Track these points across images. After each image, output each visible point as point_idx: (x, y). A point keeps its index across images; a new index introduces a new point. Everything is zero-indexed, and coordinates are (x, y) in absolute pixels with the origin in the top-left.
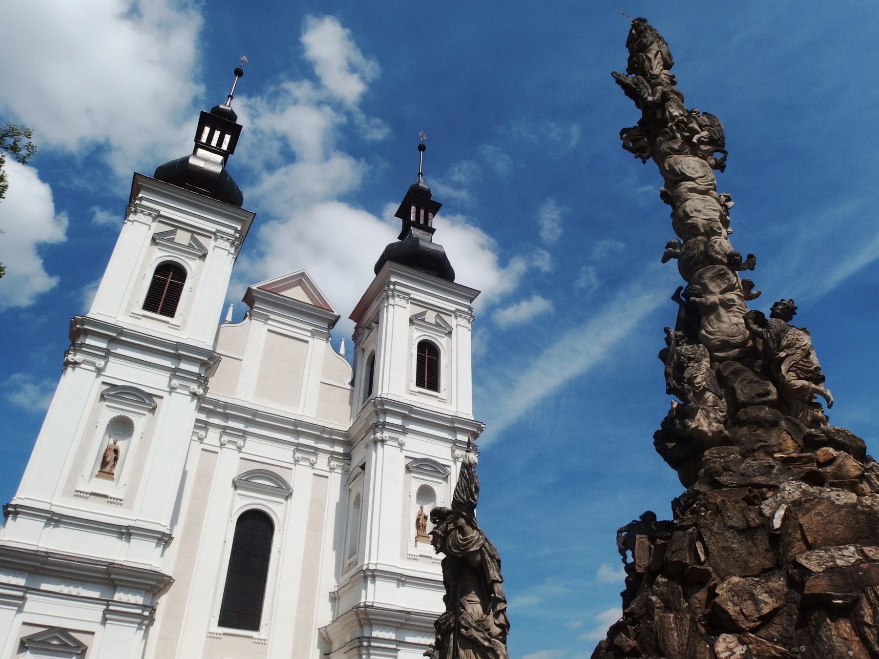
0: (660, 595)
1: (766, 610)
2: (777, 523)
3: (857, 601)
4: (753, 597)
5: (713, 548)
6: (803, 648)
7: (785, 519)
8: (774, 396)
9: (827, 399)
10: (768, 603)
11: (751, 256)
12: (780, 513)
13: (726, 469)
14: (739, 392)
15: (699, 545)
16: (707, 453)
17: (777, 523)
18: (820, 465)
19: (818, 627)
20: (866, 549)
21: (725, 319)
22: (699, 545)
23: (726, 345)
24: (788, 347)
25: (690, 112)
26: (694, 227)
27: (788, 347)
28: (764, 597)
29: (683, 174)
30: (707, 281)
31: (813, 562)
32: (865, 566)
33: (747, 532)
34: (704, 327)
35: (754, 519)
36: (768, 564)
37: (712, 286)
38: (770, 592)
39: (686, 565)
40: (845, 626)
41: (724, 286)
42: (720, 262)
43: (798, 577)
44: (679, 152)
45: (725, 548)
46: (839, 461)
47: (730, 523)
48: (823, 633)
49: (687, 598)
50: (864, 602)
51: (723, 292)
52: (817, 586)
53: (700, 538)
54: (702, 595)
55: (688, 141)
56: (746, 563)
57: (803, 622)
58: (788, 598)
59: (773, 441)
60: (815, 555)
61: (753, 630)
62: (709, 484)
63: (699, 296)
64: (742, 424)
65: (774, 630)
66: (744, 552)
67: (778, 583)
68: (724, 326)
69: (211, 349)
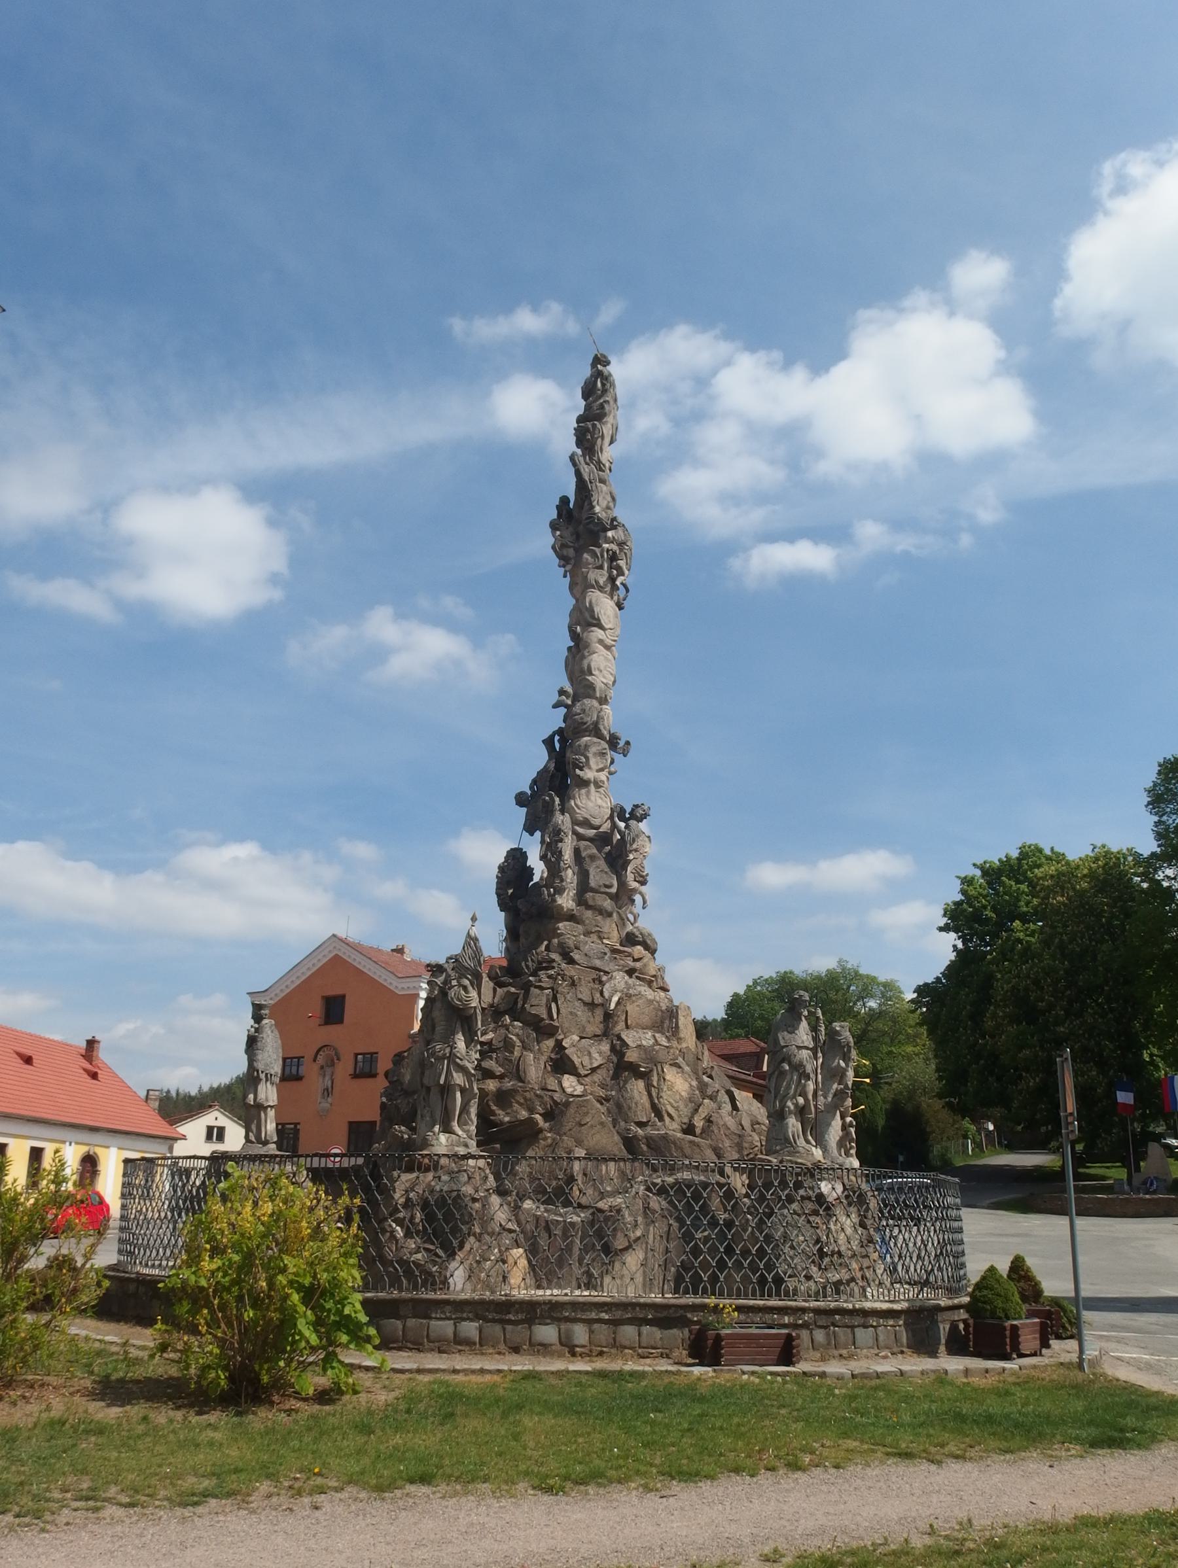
0: (517, 1035)
1: (595, 1065)
2: (612, 1006)
3: (651, 1071)
4: (589, 1054)
5: (562, 1011)
6: (613, 1093)
7: (618, 1003)
8: (614, 890)
9: (645, 902)
10: (598, 1060)
11: (628, 743)
12: (615, 999)
13: (577, 948)
14: (591, 877)
15: (553, 1005)
16: (560, 925)
17: (612, 1006)
18: (635, 960)
19: (626, 1082)
20: (657, 1035)
21: (593, 798)
22: (553, 1005)
23: (586, 823)
24: (636, 850)
25: (614, 519)
26: (591, 686)
27: (636, 850)
28: (596, 1055)
29: (599, 620)
30: (590, 755)
31: (630, 1037)
32: (657, 1048)
33: (591, 1006)
34: (574, 798)
35: (598, 999)
36: (599, 1032)
37: (592, 762)
38: (600, 1053)
39: (543, 1019)
40: (641, 1084)
41: (601, 766)
42: (601, 737)
43: (619, 1049)
44: (601, 589)
45: (571, 1013)
46: (645, 960)
47: (580, 996)
48: (628, 1086)
49: (538, 1043)
50: (655, 1073)
51: (598, 771)
52: (631, 1056)
53: (555, 999)
54: (550, 1043)
55: (612, 580)
56: (584, 1028)
57: (615, 1077)
58: (609, 1060)
59: (605, 929)
60: (632, 1033)
61: (586, 1076)
62: (561, 954)
63: (581, 770)
64: (589, 907)
65: (597, 1077)
66: (584, 1019)
67: (605, 1047)
68: (590, 804)
69: (1072, 1294)
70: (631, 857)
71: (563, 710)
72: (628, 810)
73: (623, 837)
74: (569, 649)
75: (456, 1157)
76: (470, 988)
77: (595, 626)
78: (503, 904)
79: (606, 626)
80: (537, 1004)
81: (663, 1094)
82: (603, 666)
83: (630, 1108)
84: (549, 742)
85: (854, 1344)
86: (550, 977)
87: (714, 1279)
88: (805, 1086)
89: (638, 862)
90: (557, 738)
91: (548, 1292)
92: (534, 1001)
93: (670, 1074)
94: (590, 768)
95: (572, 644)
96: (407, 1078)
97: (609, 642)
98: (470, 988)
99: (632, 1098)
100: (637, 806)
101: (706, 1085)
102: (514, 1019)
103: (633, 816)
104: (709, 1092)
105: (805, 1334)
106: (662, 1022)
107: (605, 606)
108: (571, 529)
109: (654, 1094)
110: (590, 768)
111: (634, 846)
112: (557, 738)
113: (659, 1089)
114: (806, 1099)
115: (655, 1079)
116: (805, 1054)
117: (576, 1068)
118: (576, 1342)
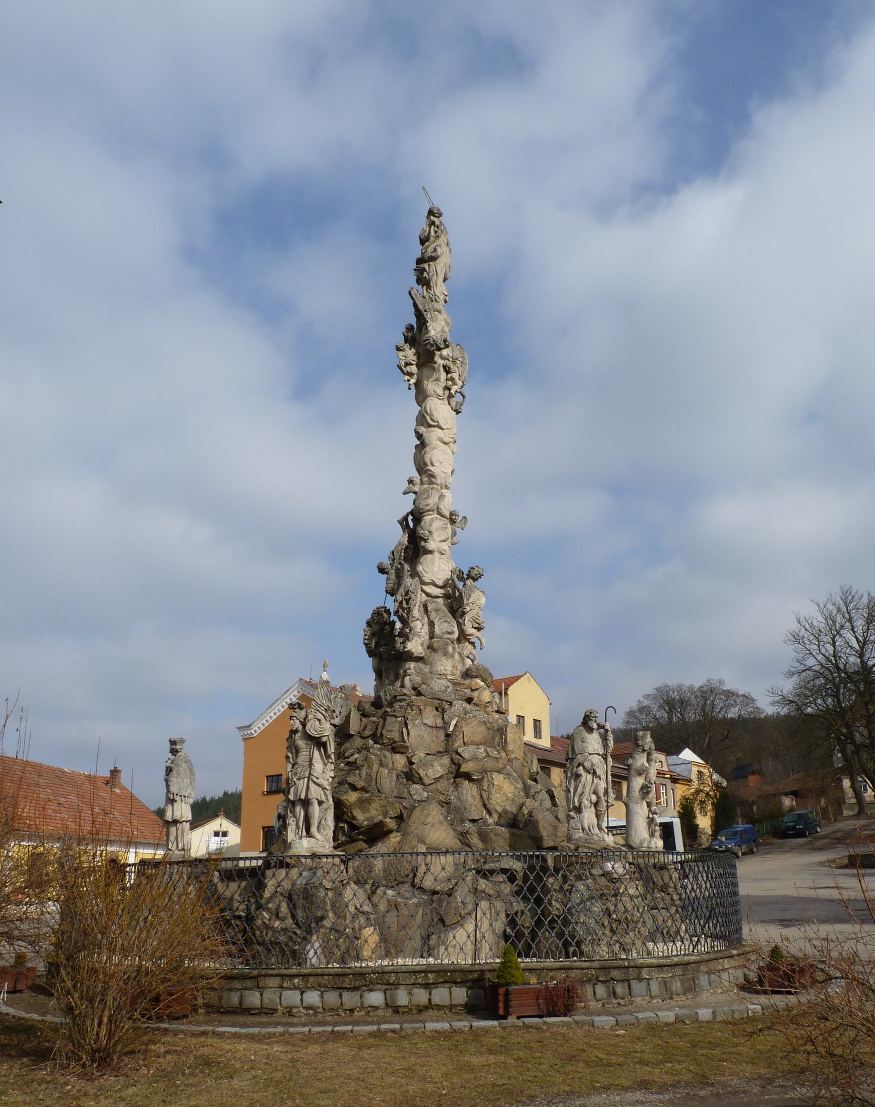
2: (451, 728)
3: (483, 778)
12: (454, 722)
14: (436, 626)
15: (405, 730)
17: (451, 728)
20: (488, 749)
22: (405, 730)
28: (439, 768)
31: (467, 752)
36: (441, 750)
37: (435, 535)
41: (443, 538)
53: (406, 725)
56: (429, 746)
67: (446, 761)
70: (468, 609)
71: (412, 496)
72: (466, 572)
73: (461, 594)
74: (417, 446)
75: (314, 856)
76: (323, 720)
77: (434, 426)
78: (371, 653)
79: (444, 427)
80: (392, 730)
81: (492, 797)
82: (441, 459)
83: (465, 808)
84: (403, 522)
85: (630, 994)
86: (401, 707)
87: (529, 947)
88: (597, 785)
89: (474, 612)
90: (410, 517)
91: (401, 961)
92: (388, 727)
93: (498, 779)
94: (434, 540)
95: (419, 442)
96: (116, 790)
97: (447, 440)
98: (323, 720)
99: (467, 801)
100: (473, 568)
101: (530, 787)
102: (376, 742)
103: (469, 576)
104: (532, 792)
105: (589, 989)
106: (493, 738)
107: (440, 409)
108: (413, 350)
109: (485, 797)
110: (434, 540)
111: (471, 600)
112: (410, 517)
113: (489, 793)
114: (598, 797)
115: (485, 784)
116: (596, 759)
117: (421, 779)
118: (399, 1003)
